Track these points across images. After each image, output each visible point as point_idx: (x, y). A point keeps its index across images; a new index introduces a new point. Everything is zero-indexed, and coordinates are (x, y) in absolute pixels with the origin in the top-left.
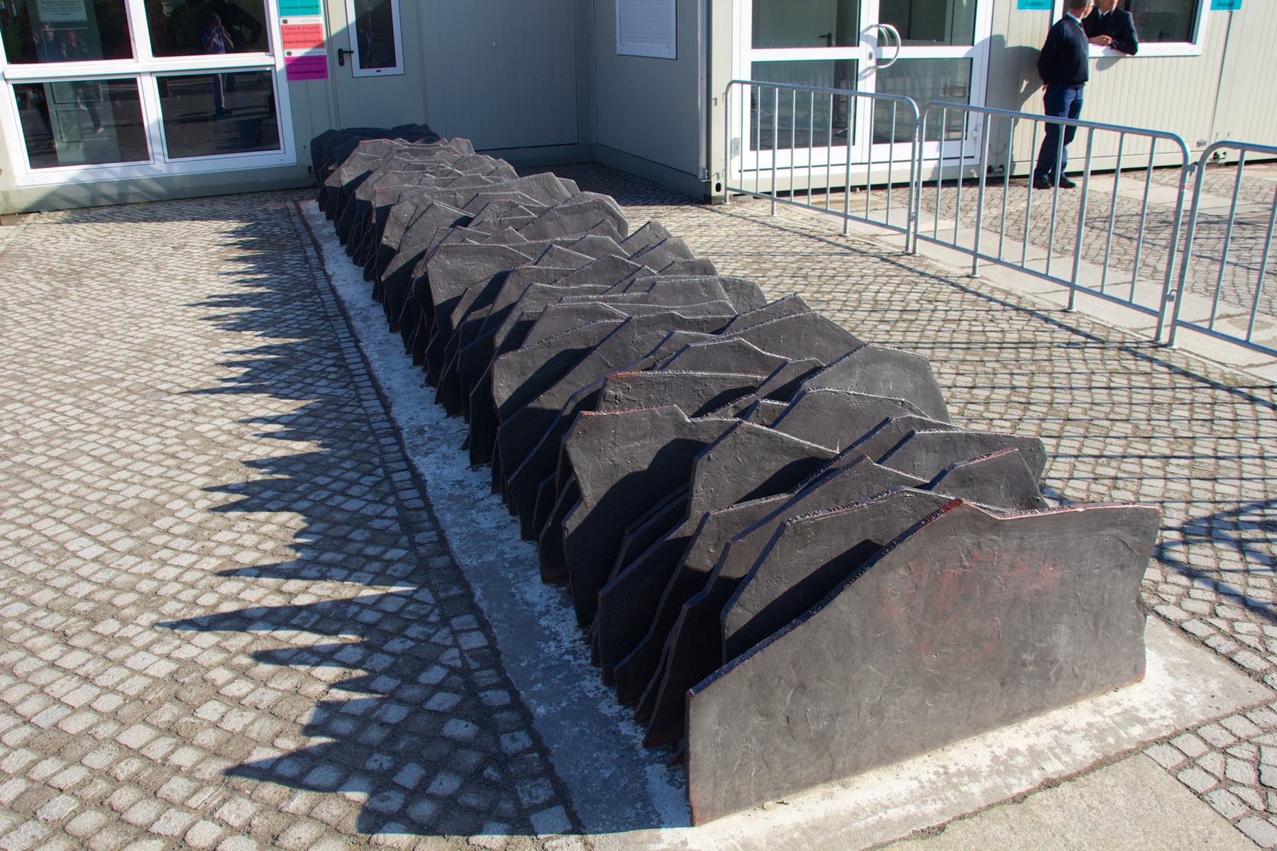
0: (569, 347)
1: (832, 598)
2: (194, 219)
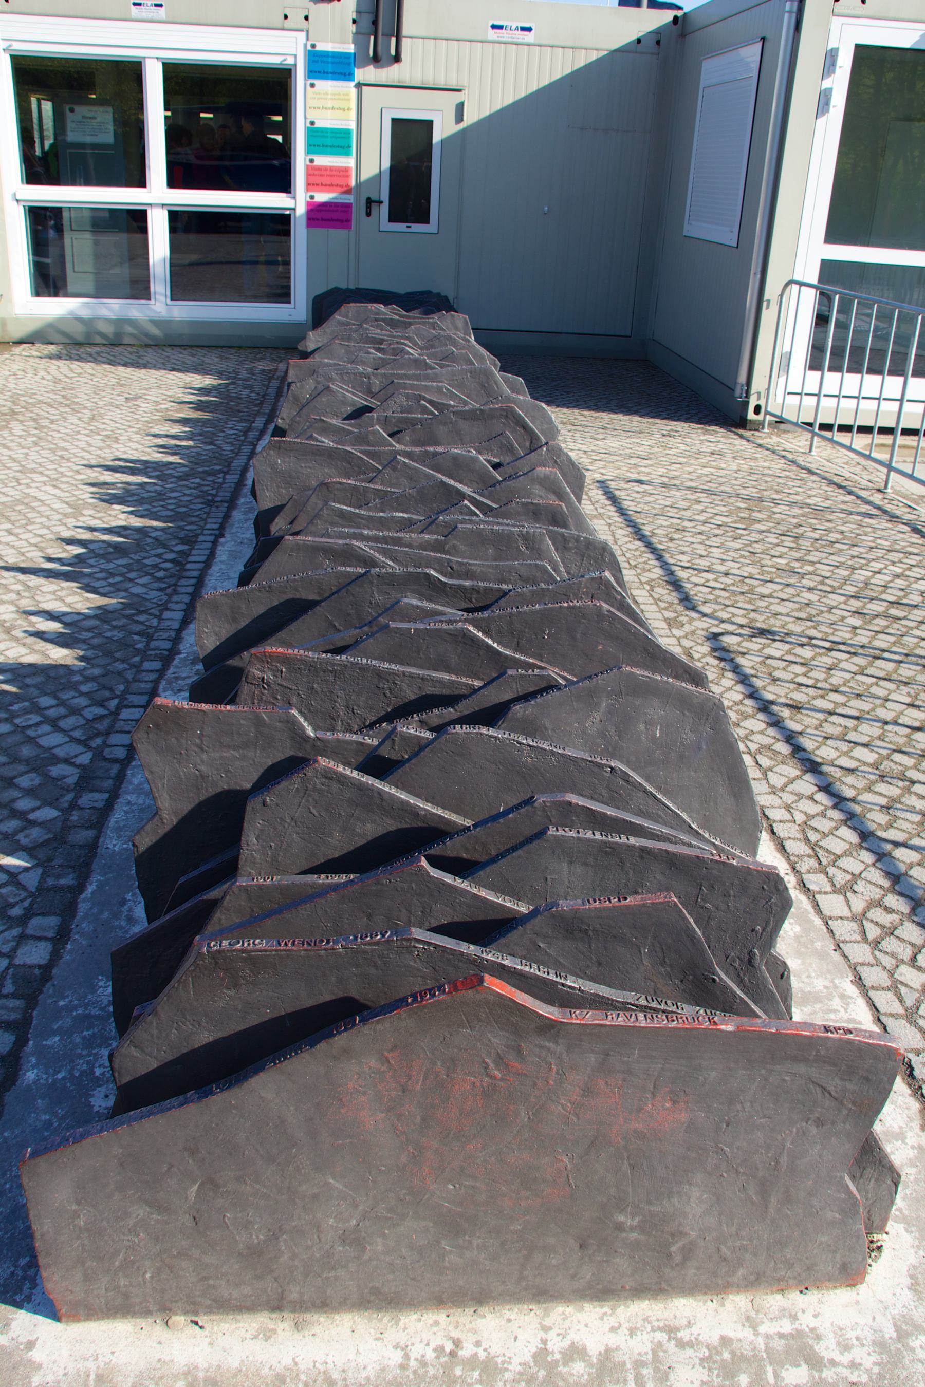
0: (297, 596)
1: (246, 1078)
2: (173, 370)
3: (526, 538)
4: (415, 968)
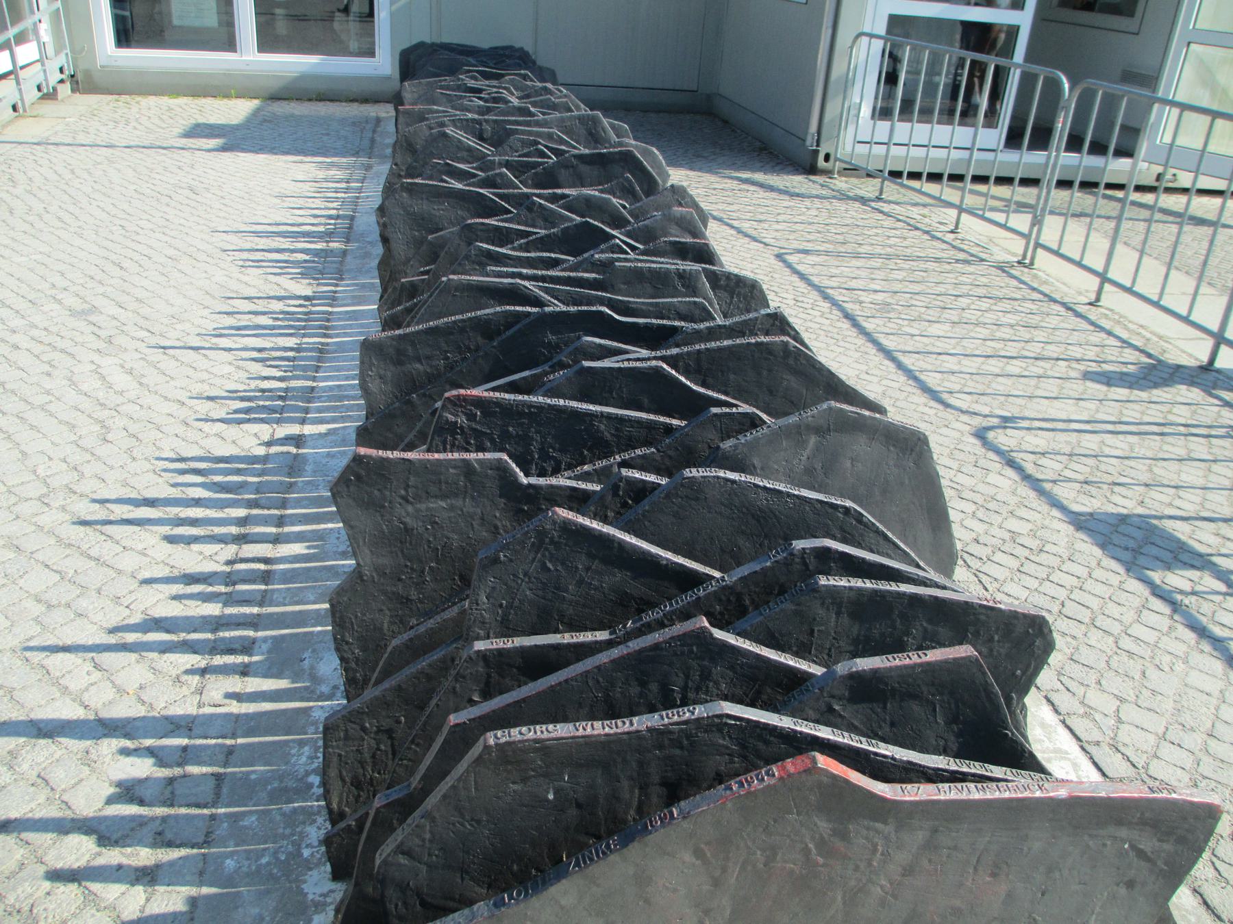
3: (681, 275)
4: (723, 746)
